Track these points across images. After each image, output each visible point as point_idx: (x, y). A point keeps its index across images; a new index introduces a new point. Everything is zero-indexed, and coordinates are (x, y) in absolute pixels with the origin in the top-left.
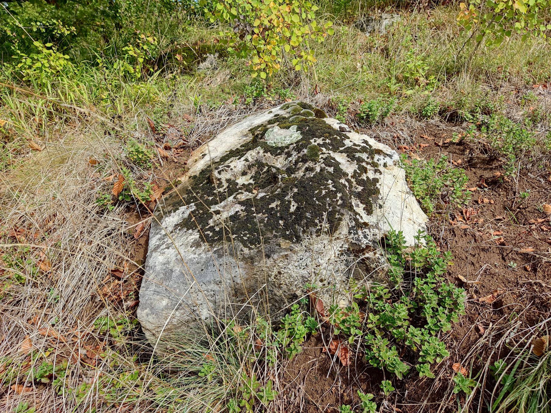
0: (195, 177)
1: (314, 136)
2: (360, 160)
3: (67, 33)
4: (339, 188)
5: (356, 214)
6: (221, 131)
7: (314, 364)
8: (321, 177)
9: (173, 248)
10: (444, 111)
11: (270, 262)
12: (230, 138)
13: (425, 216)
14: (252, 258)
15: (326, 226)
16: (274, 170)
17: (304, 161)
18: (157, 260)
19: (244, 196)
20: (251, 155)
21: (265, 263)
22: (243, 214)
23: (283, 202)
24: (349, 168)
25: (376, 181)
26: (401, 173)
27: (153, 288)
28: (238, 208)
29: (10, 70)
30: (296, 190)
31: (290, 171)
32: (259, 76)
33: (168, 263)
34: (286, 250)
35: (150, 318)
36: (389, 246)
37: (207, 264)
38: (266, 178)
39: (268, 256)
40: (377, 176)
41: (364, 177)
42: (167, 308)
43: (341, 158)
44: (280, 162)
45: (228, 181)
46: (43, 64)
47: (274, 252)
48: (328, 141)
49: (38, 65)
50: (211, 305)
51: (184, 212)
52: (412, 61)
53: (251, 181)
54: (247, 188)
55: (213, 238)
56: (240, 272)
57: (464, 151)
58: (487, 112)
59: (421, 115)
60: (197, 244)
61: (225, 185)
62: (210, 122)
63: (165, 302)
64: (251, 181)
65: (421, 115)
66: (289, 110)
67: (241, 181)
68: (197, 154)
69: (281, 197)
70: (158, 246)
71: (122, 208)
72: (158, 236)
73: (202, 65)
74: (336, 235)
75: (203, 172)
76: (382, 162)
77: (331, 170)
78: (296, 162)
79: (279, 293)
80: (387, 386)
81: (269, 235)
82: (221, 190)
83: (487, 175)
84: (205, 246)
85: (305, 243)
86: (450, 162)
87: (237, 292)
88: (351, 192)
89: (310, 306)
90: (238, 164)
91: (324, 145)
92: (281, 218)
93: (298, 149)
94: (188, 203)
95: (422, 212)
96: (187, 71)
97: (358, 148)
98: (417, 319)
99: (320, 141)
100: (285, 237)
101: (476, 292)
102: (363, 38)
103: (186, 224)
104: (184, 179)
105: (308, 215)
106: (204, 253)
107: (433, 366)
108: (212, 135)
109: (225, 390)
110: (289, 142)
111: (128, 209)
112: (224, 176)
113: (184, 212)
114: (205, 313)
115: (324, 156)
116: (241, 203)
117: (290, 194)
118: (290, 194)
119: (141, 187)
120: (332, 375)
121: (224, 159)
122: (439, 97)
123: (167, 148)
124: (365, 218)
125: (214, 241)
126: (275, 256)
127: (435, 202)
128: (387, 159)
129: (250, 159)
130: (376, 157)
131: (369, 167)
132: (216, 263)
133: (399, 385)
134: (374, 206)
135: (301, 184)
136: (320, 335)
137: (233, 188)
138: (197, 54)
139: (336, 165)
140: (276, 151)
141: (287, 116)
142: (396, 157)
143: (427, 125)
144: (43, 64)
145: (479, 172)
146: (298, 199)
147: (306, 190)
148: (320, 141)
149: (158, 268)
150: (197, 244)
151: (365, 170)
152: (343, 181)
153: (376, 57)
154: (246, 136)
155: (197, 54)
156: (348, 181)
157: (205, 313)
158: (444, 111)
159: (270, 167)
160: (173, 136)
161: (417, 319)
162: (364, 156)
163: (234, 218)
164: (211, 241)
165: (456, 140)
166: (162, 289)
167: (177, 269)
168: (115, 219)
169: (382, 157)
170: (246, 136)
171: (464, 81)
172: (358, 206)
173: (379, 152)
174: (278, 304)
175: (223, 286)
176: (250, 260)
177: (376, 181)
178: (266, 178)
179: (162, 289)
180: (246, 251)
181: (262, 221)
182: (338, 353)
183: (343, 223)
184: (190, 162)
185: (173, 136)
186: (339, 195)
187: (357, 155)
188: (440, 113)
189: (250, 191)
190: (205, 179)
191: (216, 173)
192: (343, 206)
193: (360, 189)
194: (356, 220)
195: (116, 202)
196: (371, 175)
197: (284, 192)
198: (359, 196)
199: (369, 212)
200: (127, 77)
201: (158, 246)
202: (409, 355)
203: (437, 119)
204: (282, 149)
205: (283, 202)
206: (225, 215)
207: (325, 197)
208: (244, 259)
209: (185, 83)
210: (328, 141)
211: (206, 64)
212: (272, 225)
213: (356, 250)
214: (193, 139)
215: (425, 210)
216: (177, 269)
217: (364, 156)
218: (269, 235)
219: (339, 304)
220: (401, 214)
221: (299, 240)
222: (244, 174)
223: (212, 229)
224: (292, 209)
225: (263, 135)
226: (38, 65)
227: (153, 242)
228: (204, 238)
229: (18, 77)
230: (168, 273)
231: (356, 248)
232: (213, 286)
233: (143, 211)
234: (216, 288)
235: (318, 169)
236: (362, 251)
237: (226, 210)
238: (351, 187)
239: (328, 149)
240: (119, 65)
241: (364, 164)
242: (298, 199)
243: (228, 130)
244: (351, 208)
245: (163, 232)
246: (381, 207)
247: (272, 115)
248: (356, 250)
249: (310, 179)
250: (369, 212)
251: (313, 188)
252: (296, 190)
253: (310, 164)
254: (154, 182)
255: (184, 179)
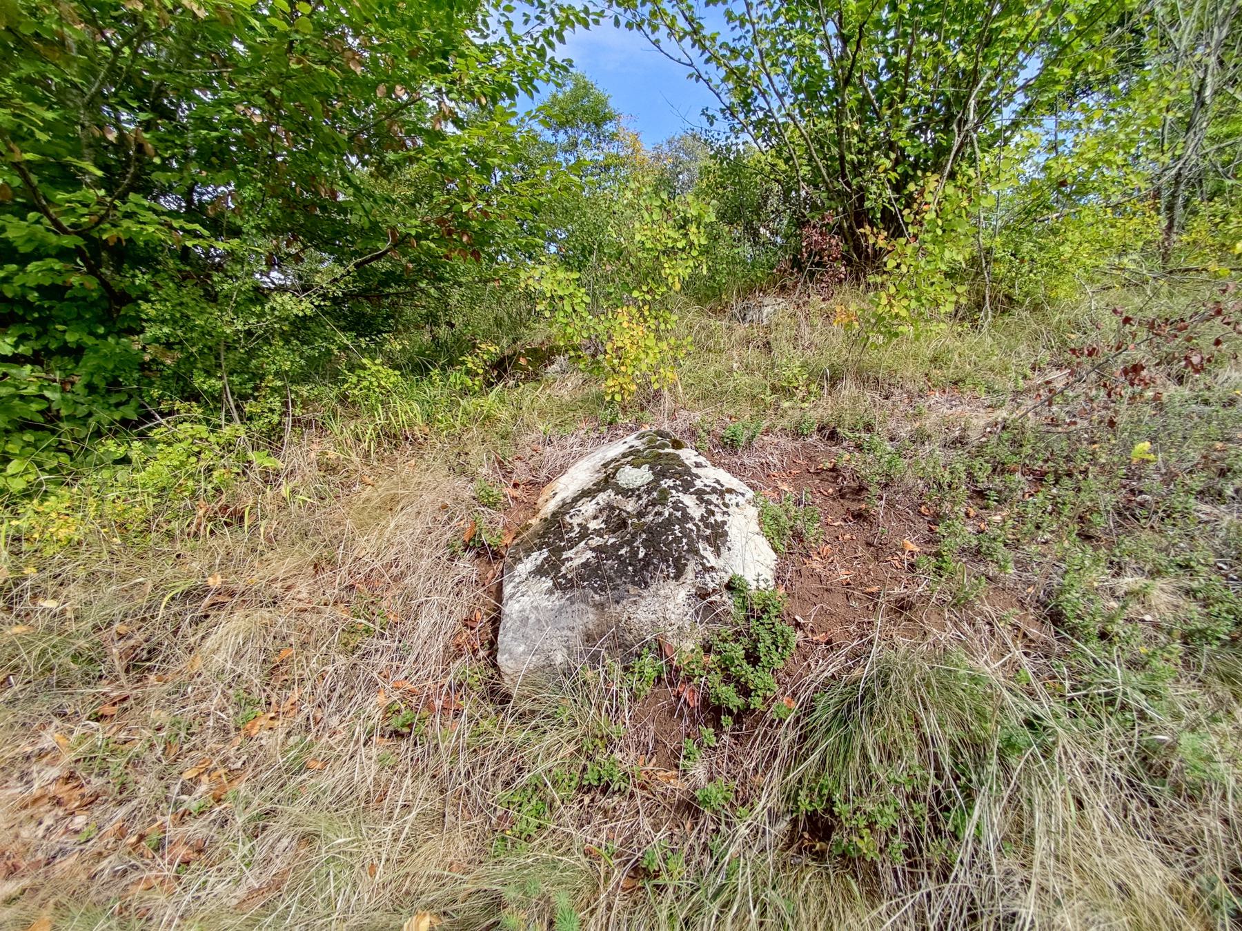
0: (546, 520)
1: (664, 477)
2: (709, 502)
3: (399, 347)
4: (686, 533)
5: (704, 557)
6: (573, 464)
7: (664, 706)
8: (669, 522)
9: (528, 597)
10: (823, 428)
11: (619, 608)
12: (580, 475)
13: (774, 556)
14: (602, 605)
15: (672, 571)
16: (625, 515)
17: (654, 505)
18: (512, 608)
19: (596, 541)
20: (602, 498)
21: (614, 610)
22: (594, 561)
23: (632, 548)
24: (696, 512)
25: (724, 523)
26: (753, 512)
27: (511, 634)
28: (589, 554)
29: (336, 391)
30: (644, 536)
31: (640, 515)
32: (613, 398)
33: (524, 610)
34: (634, 596)
35: (510, 663)
36: (734, 589)
37: (560, 611)
38: (617, 523)
39: (618, 602)
40: (726, 518)
41: (712, 520)
42: (524, 653)
43: (689, 500)
44: (630, 506)
45: (579, 525)
46: (371, 383)
47: (623, 598)
48: (678, 482)
49: (366, 383)
50: (565, 650)
51: (537, 558)
52: (791, 365)
53: (603, 526)
54: (598, 533)
55: (563, 586)
56: (591, 617)
57: (837, 478)
58: (869, 428)
59: (797, 433)
60: (550, 592)
61: (577, 529)
62: (561, 454)
63: (521, 649)
64: (603, 526)
65: (797, 433)
66: (644, 440)
67: (593, 525)
68: (547, 492)
69: (630, 543)
70: (514, 594)
71: (472, 554)
72: (512, 584)
73: (549, 369)
74: (682, 580)
75: (554, 514)
76: (734, 502)
77: (679, 514)
78: (647, 506)
79: (629, 637)
80: (726, 720)
81: (619, 582)
82: (573, 535)
83: (854, 507)
84: (558, 593)
85: (653, 588)
86: (817, 495)
87: (589, 638)
88: (699, 536)
89: (660, 652)
90: (588, 507)
91: (674, 487)
92: (630, 564)
93: (649, 492)
94: (540, 549)
95: (772, 553)
96: (535, 377)
97: (708, 489)
98: (752, 658)
99: (670, 483)
100: (634, 583)
101: (812, 631)
102: (741, 330)
103: (539, 571)
104: (534, 521)
105: (655, 561)
106: (557, 600)
107: (765, 698)
108: (563, 469)
109: (579, 732)
110: (640, 483)
111: (478, 555)
112: (576, 521)
113: (537, 558)
114: (559, 658)
115: (673, 500)
116: (593, 550)
117: (639, 540)
118: (639, 540)
119: (491, 532)
120: (681, 716)
121: (576, 500)
122: (819, 410)
123: (516, 485)
124: (712, 560)
125: (566, 588)
126: (624, 602)
127: (789, 540)
128: (740, 498)
129: (601, 503)
130: (728, 496)
131: (716, 510)
132: (569, 610)
133: (738, 719)
134: (722, 549)
135: (649, 530)
136: (673, 676)
137: (584, 534)
138: (542, 356)
139: (684, 510)
140: (627, 493)
141: (641, 448)
142: (750, 494)
143: (803, 446)
144: (371, 383)
145: (847, 503)
146: (648, 544)
147: (654, 535)
148: (670, 483)
149: (514, 616)
150: (550, 592)
151: (713, 513)
152: (690, 525)
153: (752, 355)
154: (598, 472)
155: (542, 356)
156: (695, 524)
157: (559, 658)
158: (823, 428)
159: (621, 510)
160: (521, 473)
161: (752, 658)
162: (714, 498)
163: (585, 565)
164: (564, 589)
165: (830, 466)
166: (519, 635)
167: (533, 617)
168: (466, 566)
169: (734, 496)
170: (598, 472)
171: (848, 388)
172: (705, 549)
173: (730, 491)
174: (627, 649)
175: (576, 631)
176: (600, 606)
177: (724, 523)
178: (617, 523)
179: (519, 635)
180: (597, 597)
181: (612, 568)
182: (685, 695)
183: (689, 568)
184: (540, 501)
185: (521, 473)
186: (685, 541)
187: (706, 497)
188: (820, 430)
189: (601, 536)
190: (556, 523)
191: (567, 517)
192: (688, 551)
193: (708, 532)
194: (703, 564)
195: (467, 547)
196: (719, 518)
197: (634, 536)
198: (707, 539)
199: (718, 553)
200: (465, 392)
201: (514, 594)
202: (745, 691)
203: (815, 437)
204: (633, 490)
205: (632, 548)
206: (577, 562)
207: (671, 543)
208: (595, 605)
209: (528, 393)
210: (678, 482)
211: (555, 367)
212: (622, 572)
213: (702, 594)
214: (543, 473)
215: (776, 550)
216: (533, 617)
217: (714, 498)
218: (619, 582)
219: (687, 648)
220: (750, 557)
221: (647, 585)
222: (595, 517)
223: (564, 576)
224: (641, 555)
225: (614, 474)
226: (366, 383)
227: (508, 590)
228: (557, 586)
229: (343, 399)
230: (524, 621)
231: (703, 592)
232: (567, 632)
233: (497, 556)
234: (569, 633)
235: (667, 514)
236: (709, 595)
237: (578, 556)
238: (698, 530)
239: (678, 491)
240: (455, 377)
241: (712, 507)
242: (648, 544)
243: (580, 463)
244: (697, 552)
245: (517, 580)
246: (729, 549)
247: (627, 446)
248: (702, 594)
249: (658, 525)
250: (718, 553)
251: (660, 534)
252: (644, 536)
253: (658, 508)
254: (505, 527)
255: (534, 521)
